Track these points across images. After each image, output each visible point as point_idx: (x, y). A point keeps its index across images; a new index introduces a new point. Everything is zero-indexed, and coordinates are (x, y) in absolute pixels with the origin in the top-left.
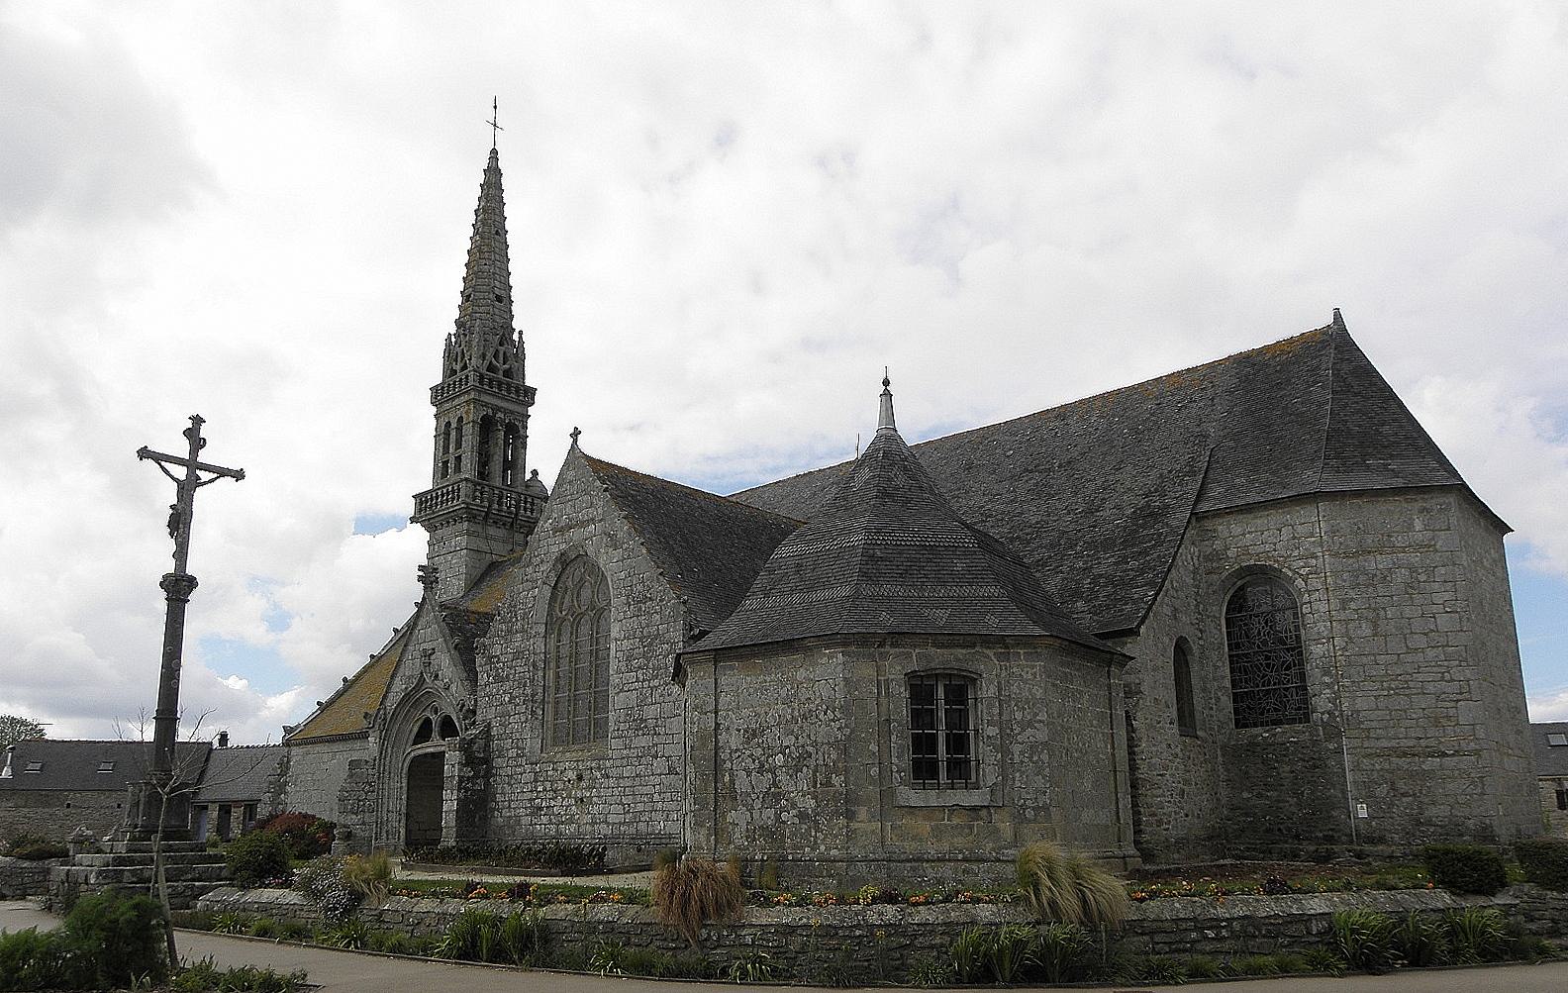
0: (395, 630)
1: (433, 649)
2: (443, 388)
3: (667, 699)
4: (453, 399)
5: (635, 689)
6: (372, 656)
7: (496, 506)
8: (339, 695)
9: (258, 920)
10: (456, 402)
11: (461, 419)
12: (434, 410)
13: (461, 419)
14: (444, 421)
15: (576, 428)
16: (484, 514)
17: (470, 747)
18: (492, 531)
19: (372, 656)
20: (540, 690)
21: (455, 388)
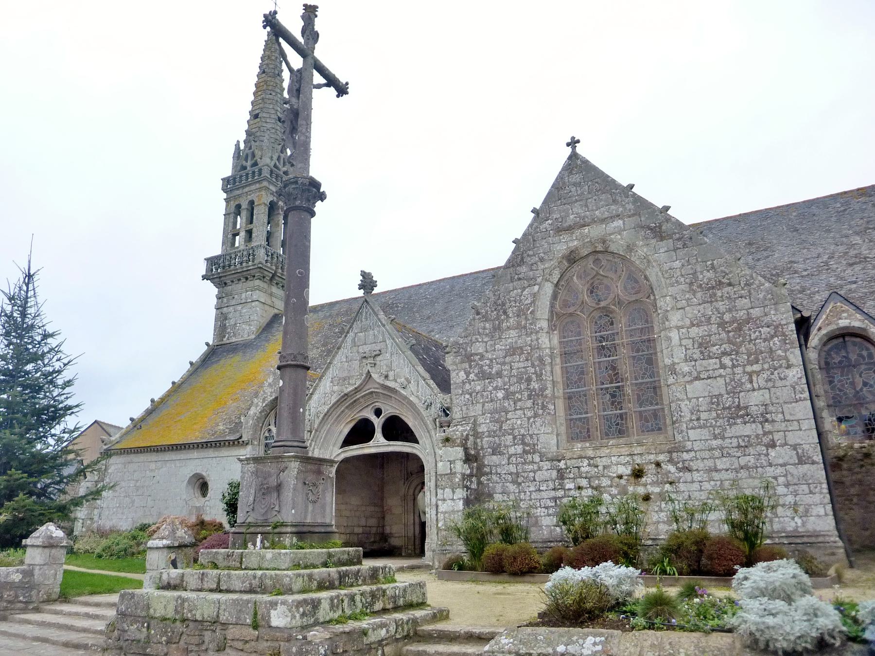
0: (191, 363)
1: (380, 351)
2: (234, 179)
3: (779, 383)
4: (243, 187)
5: (720, 376)
6: (173, 383)
7: (280, 271)
8: (149, 413)
9: (18, 620)
10: (247, 189)
11: (252, 203)
12: (225, 196)
13: (252, 203)
14: (233, 204)
15: (573, 138)
16: (271, 275)
17: (466, 443)
18: (274, 289)
19: (173, 383)
20: (549, 385)
21: (247, 178)
